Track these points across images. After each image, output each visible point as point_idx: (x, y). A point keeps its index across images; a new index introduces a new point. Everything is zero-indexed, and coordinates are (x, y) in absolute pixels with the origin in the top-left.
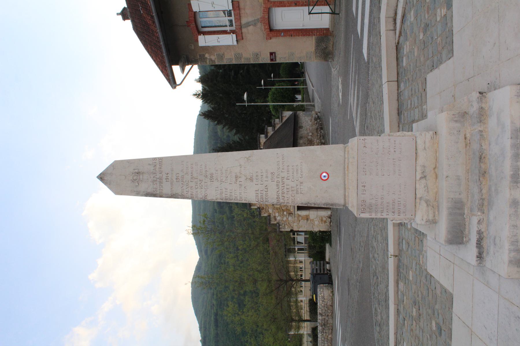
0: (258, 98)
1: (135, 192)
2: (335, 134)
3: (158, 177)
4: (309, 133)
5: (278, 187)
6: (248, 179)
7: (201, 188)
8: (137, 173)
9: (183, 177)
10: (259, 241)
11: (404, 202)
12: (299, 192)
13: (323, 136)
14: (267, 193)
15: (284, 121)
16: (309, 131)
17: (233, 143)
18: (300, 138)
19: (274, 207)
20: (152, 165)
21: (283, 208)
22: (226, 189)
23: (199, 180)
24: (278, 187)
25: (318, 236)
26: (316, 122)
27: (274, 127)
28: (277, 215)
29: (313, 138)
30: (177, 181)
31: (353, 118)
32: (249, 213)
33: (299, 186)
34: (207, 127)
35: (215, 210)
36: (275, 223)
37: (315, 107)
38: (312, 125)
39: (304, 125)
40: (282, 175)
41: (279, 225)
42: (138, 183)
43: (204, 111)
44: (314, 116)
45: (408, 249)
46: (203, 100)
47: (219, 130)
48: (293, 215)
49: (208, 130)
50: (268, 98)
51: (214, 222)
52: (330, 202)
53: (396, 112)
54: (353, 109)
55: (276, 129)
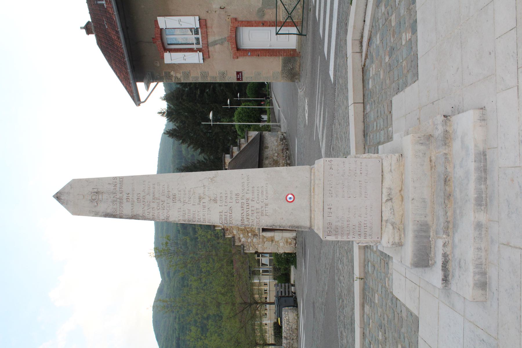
0: (223, 118)
1: (94, 213)
3: (118, 197)
4: (274, 154)
5: (243, 209)
7: (163, 209)
8: (97, 193)
9: (144, 197)
11: (371, 225)
12: (264, 214)
13: (288, 156)
15: (249, 141)
16: (274, 152)
22: (189, 210)
25: (283, 258)
26: (281, 143)
28: (241, 236)
29: (278, 159)
31: (319, 140)
34: (172, 146)
35: (179, 231)
36: (240, 244)
37: (280, 127)
38: (278, 146)
39: (269, 145)
40: (247, 196)
41: (244, 247)
42: (97, 203)
43: (169, 130)
45: (373, 272)
46: (168, 119)
49: (173, 149)
51: (177, 244)
52: (296, 225)
53: (361, 134)
55: (241, 149)
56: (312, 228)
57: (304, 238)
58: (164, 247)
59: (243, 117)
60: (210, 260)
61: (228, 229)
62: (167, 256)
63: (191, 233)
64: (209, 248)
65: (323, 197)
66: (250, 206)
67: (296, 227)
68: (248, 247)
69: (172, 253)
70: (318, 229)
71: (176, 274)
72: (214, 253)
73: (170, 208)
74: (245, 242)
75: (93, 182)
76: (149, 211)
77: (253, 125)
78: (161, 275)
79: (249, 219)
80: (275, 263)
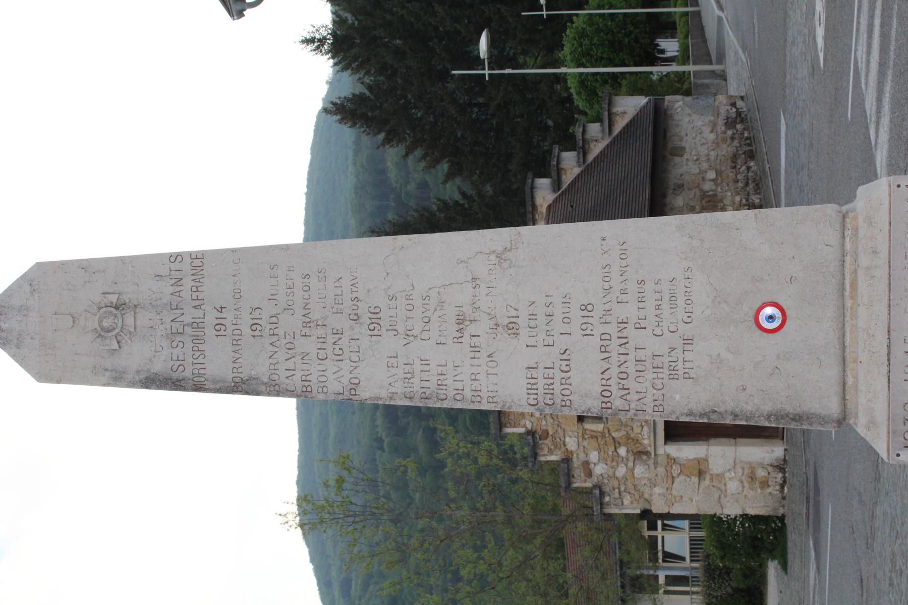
0: (525, 53)
1: (108, 374)
2: (798, 173)
3: (187, 319)
5: (606, 355)
6: (500, 329)
7: (339, 358)
8: (116, 308)
9: (274, 320)
10: (529, 548)
12: (681, 372)
14: (568, 375)
15: (618, 128)
16: (705, 165)
17: (439, 210)
18: (675, 189)
19: (585, 430)
20: (168, 278)
21: (613, 434)
22: (425, 362)
23: (330, 332)
24: (606, 355)
25: (738, 534)
26: (730, 133)
27: (584, 152)
28: (594, 456)
29: (719, 190)
30: (256, 333)
31: (866, 117)
32: (495, 452)
33: (678, 353)
34: (351, 154)
35: (379, 440)
36: (588, 484)
37: (726, 80)
38: (718, 145)
39: (687, 143)
40: (621, 312)
41: (602, 494)
42: (118, 342)
43: (340, 98)
44: (723, 110)
46: (336, 60)
47: (390, 165)
48: (649, 457)
49: (354, 164)
50: (563, 50)
51: (373, 484)
52: (789, 409)
54: (866, 84)
55: (591, 158)
56: (847, 421)
57: (811, 463)
58: (333, 495)
59: (592, 49)
60: (487, 539)
61: (548, 433)
62: (342, 526)
63: (422, 449)
64: (483, 498)
65: (887, 312)
66: (631, 345)
67: (791, 416)
68: (617, 495)
69: (359, 515)
70: (872, 424)
71: (371, 588)
72: (500, 514)
73: (360, 354)
74: (605, 476)
75: (104, 271)
76: (290, 364)
77: (627, 76)
78: (320, 589)
79: (627, 391)
80: (712, 550)
